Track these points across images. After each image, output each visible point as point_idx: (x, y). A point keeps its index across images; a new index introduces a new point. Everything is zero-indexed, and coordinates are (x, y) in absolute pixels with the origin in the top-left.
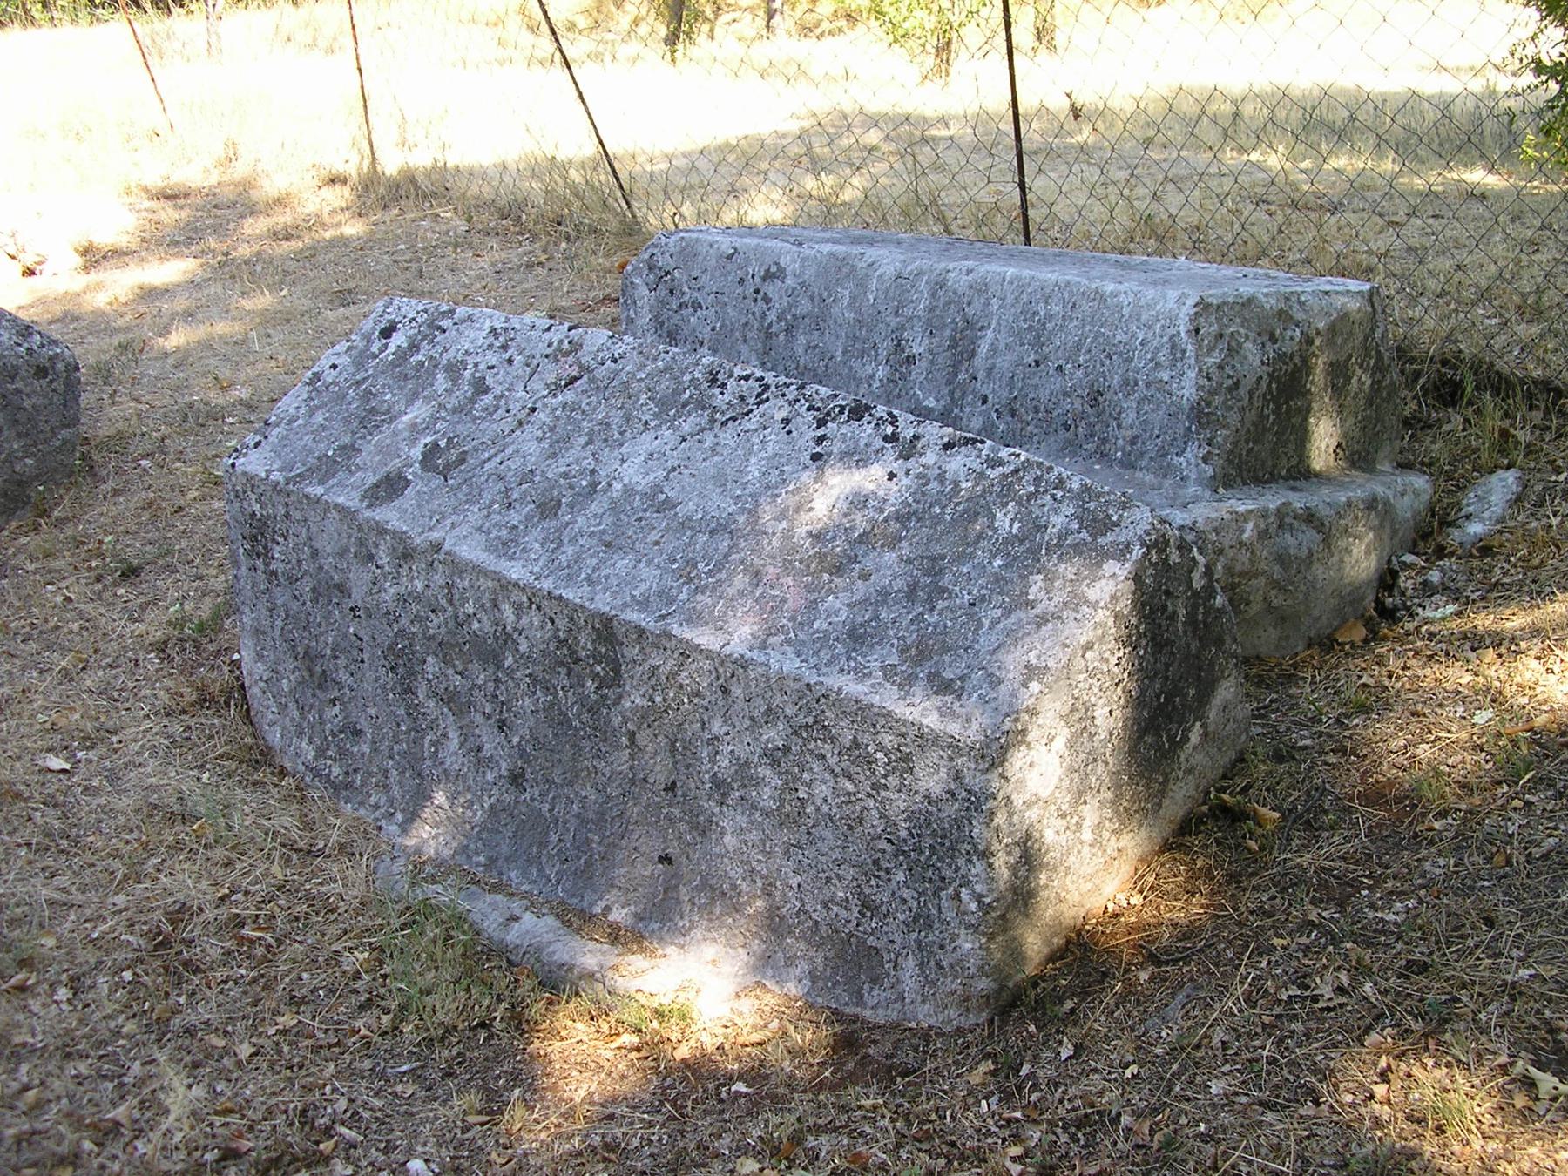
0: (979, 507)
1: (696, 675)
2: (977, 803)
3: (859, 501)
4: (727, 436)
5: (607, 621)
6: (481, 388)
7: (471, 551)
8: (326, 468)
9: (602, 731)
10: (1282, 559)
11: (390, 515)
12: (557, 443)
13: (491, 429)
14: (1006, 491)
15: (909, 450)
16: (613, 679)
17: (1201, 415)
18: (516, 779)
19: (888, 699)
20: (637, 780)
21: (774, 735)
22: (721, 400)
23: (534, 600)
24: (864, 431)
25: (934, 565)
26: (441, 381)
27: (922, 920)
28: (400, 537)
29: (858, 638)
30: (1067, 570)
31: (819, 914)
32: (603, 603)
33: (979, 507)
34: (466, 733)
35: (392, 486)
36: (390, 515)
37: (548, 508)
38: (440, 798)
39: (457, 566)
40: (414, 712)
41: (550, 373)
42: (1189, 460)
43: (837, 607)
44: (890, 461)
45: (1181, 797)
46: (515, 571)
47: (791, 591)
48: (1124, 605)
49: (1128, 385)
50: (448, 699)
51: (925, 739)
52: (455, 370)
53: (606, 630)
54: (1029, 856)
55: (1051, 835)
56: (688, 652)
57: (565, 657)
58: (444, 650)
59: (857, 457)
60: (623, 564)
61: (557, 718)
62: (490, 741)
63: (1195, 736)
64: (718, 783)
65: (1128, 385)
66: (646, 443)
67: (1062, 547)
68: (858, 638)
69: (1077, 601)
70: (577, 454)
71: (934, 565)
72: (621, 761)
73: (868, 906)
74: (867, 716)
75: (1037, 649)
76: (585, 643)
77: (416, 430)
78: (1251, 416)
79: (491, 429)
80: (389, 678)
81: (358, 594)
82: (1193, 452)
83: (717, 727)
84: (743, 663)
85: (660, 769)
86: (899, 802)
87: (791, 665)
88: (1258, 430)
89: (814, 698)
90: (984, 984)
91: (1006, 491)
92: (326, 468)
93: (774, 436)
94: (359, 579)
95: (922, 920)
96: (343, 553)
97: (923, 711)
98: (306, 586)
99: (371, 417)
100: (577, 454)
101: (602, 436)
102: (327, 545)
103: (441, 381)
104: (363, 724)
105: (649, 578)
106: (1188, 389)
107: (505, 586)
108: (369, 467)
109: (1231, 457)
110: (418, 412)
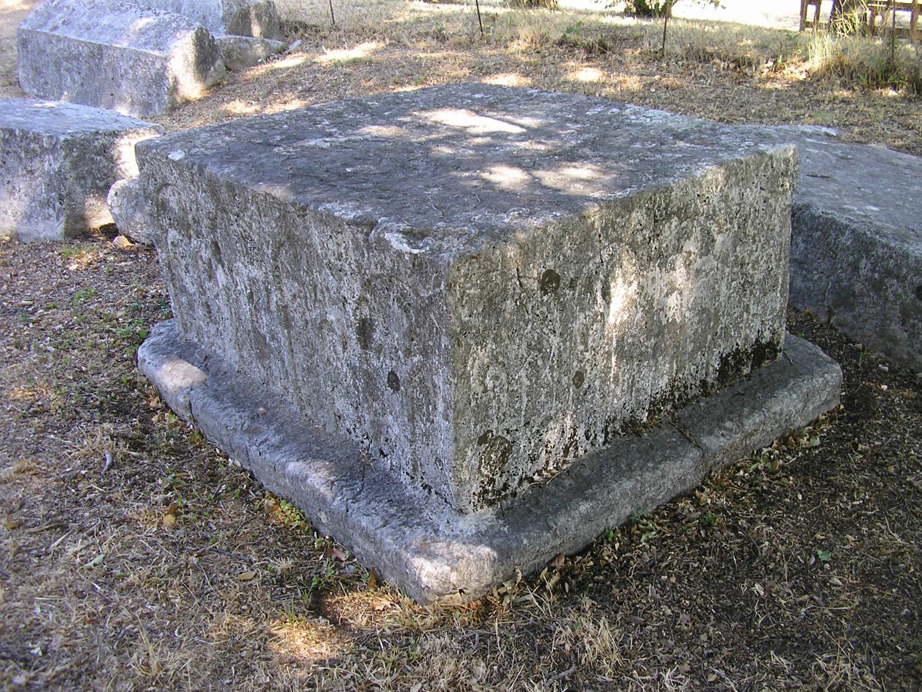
0: (170, 23)
1: (117, 54)
2: (165, 68)
3: (148, 24)
4: (124, 15)
5: (100, 45)
6: (74, 10)
7: (73, 37)
8: (40, 26)
9: (99, 69)
10: (240, 48)
11: (56, 33)
12: (90, 18)
13: (76, 17)
14: (175, 20)
15: (158, 15)
16: (102, 58)
17: (224, 19)
18: (82, 85)
19: (151, 52)
20: (106, 79)
21: (131, 63)
22: (123, 8)
23: (86, 44)
24: (150, 12)
25: (160, 32)
26: (65, 9)
27: (158, 95)
28: (58, 36)
29: (146, 44)
30: (184, 32)
31: (140, 98)
32: (99, 42)
33: (170, 23)
34: (72, 77)
35: (56, 28)
36: (56, 33)
37: (88, 29)
38: (66, 93)
39: (70, 40)
40: (60, 75)
41: (89, 6)
42: (221, 29)
43: (143, 40)
44: (154, 16)
45: (210, 81)
46: (82, 39)
47: (134, 37)
48: (194, 38)
49: (210, 14)
50: (68, 70)
51: (157, 58)
52: (68, 7)
53: (100, 48)
54: (176, 81)
55: (181, 79)
56: (115, 49)
57: (92, 55)
58: (67, 59)
59: (148, 16)
60: (103, 36)
61: (90, 69)
62: (76, 77)
63: (212, 69)
64: (122, 76)
65: (210, 14)
66: (108, 17)
67: (183, 28)
68: (146, 44)
69: (185, 36)
70: (94, 19)
71: (160, 32)
72: (103, 75)
73: (149, 94)
74: (146, 55)
75: (178, 43)
76: (96, 51)
77: (60, 18)
78: (235, 20)
79: (76, 17)
80: (54, 68)
81: (48, 51)
82: (222, 27)
83: (121, 64)
84: (125, 49)
85: (110, 75)
86: (153, 71)
87: (134, 48)
88: (237, 24)
89: (138, 54)
90: (169, 105)
91: (175, 20)
92: (40, 26)
93: (133, 14)
94: (48, 49)
95: (158, 95)
96: (45, 43)
97: (157, 53)
98: (36, 52)
99: (50, 16)
100: (94, 19)
101: (99, 16)
102: (41, 42)
103: (65, 9)
104: (49, 81)
105: (108, 38)
106: (221, 15)
107: (80, 42)
108: (51, 24)
109: (230, 28)
110: (60, 15)
